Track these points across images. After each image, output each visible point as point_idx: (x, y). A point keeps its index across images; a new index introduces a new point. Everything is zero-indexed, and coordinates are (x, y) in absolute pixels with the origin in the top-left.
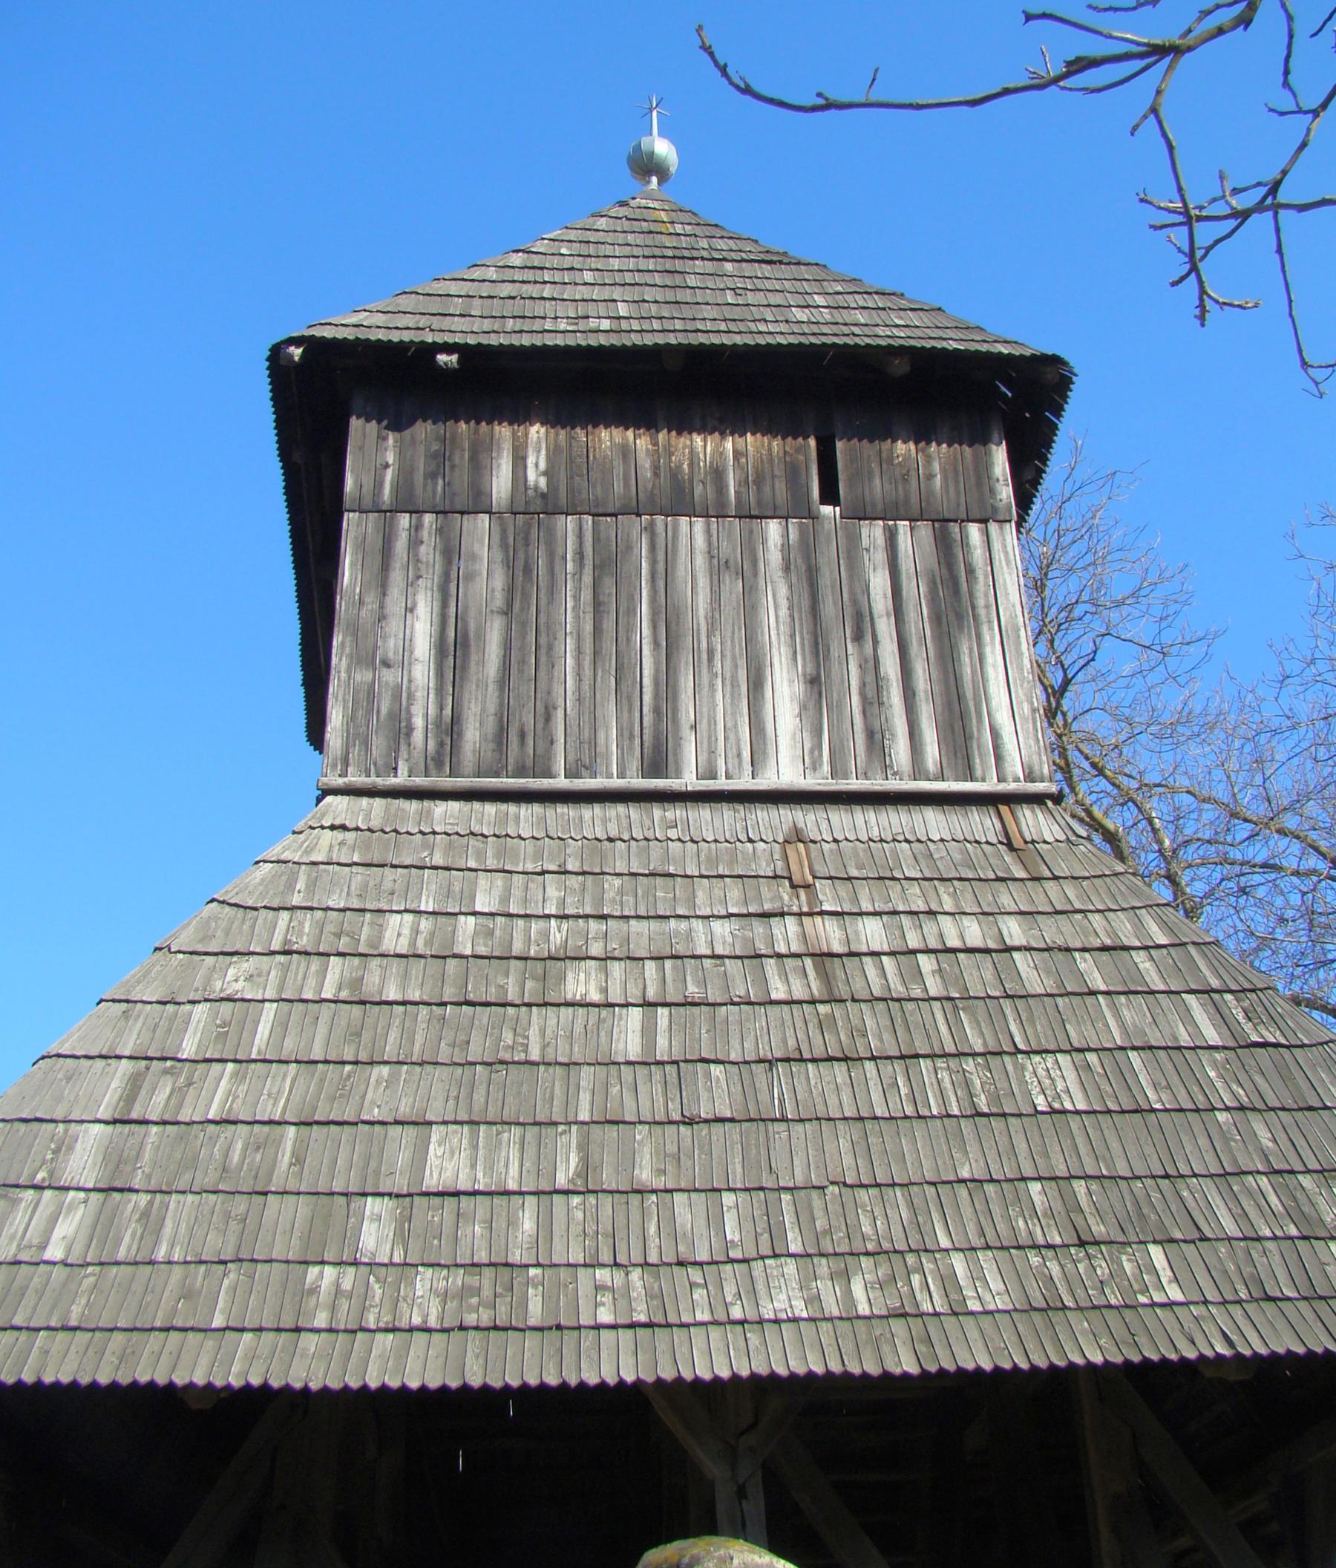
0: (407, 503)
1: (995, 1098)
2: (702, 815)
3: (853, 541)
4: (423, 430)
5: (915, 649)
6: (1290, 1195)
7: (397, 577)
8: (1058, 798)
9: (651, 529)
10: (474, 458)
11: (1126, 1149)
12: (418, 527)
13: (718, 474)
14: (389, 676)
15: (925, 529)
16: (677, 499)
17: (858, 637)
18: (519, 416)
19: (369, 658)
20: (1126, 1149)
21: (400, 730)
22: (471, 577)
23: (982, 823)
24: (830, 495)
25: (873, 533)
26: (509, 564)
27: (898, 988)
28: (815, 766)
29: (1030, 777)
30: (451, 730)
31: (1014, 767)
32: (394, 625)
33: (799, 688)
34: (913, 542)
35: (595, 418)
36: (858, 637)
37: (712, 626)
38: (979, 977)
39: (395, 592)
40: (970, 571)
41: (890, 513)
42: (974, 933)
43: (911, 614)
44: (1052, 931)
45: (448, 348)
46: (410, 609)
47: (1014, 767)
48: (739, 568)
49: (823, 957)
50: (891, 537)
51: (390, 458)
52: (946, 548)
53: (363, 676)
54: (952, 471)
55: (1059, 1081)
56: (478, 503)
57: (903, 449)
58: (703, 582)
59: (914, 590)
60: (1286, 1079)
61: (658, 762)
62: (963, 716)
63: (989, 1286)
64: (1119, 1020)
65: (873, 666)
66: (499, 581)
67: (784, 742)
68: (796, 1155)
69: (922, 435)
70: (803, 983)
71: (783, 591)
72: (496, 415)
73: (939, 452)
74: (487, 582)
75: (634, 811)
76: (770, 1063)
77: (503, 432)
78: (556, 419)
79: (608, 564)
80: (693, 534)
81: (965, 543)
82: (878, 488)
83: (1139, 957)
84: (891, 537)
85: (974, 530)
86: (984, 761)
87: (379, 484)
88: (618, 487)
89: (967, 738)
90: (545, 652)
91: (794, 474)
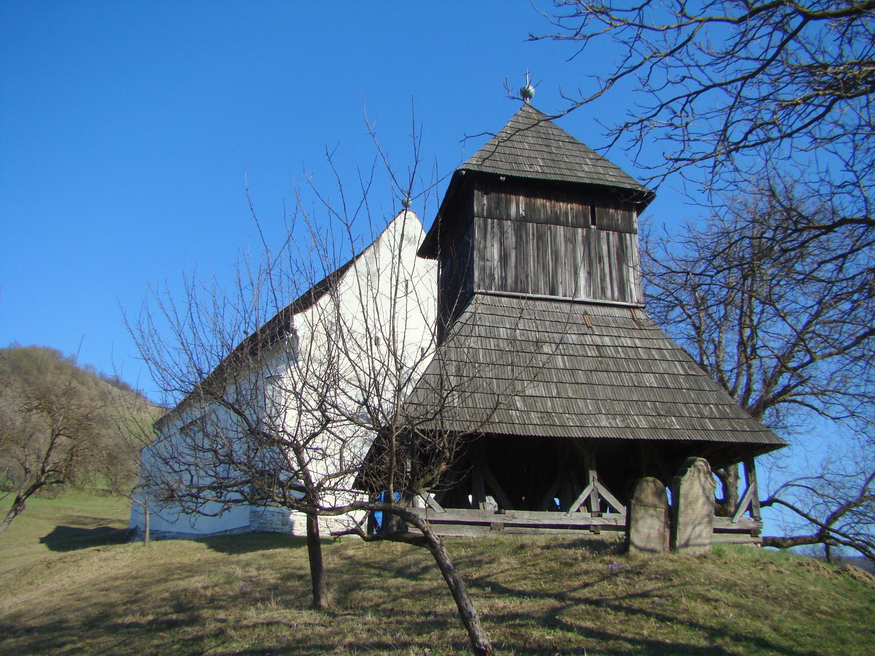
0: (490, 216)
1: (638, 383)
2: (563, 305)
3: (599, 235)
4: (493, 195)
5: (613, 266)
6: (698, 408)
7: (488, 236)
8: (644, 308)
9: (550, 228)
10: (506, 205)
11: (666, 397)
12: (493, 223)
13: (566, 214)
14: (488, 263)
15: (616, 234)
16: (556, 220)
17: (600, 263)
18: (517, 194)
19: (483, 258)
20: (666, 397)
21: (492, 276)
22: (507, 238)
23: (627, 313)
24: (594, 223)
25: (603, 234)
26: (516, 235)
27: (615, 356)
28: (589, 295)
29: (638, 302)
30: (504, 279)
31: (635, 299)
32: (488, 250)
33: (586, 275)
34: (614, 237)
35: (537, 196)
36: (600, 263)
37: (565, 256)
38: (631, 353)
39: (488, 241)
40: (627, 247)
41: (608, 229)
42: (629, 342)
43: (612, 257)
44: (647, 344)
45: (503, 176)
46: (493, 246)
47: (635, 299)
48: (571, 240)
49: (597, 346)
50: (608, 235)
51: (485, 202)
52: (621, 240)
53: (482, 263)
54: (623, 218)
55: (650, 380)
56: (508, 218)
57: (611, 211)
58: (563, 244)
59: (613, 250)
60: (697, 383)
61: (553, 291)
62: (624, 285)
63: (643, 423)
64: (662, 367)
65: (603, 270)
66: (514, 240)
67: (582, 288)
68: (601, 393)
69: (616, 208)
70: (594, 353)
71: (582, 248)
72: (511, 193)
73: (620, 212)
74: (511, 240)
75: (548, 303)
76: (591, 371)
77: (513, 197)
78: (526, 195)
79: (540, 237)
80: (561, 230)
81: (626, 239)
82: (605, 221)
83: (665, 351)
84: (608, 235)
85: (628, 235)
86: (628, 297)
87: (483, 210)
88: (542, 216)
89: (624, 291)
90: (526, 260)
91: (585, 216)
